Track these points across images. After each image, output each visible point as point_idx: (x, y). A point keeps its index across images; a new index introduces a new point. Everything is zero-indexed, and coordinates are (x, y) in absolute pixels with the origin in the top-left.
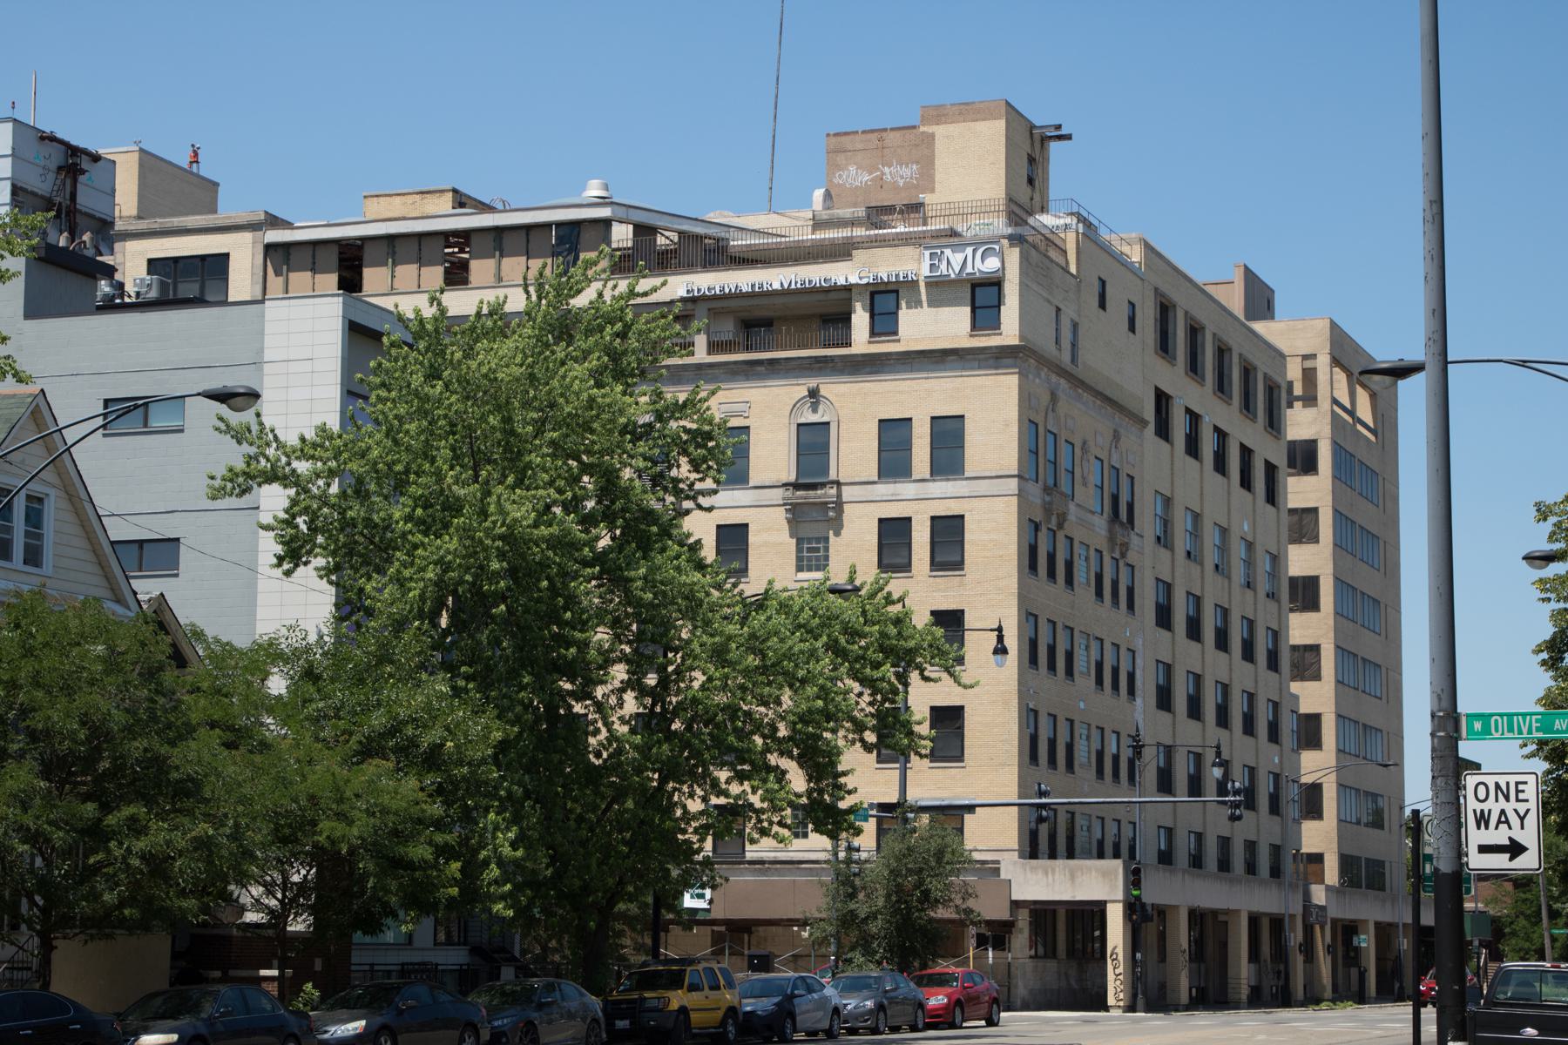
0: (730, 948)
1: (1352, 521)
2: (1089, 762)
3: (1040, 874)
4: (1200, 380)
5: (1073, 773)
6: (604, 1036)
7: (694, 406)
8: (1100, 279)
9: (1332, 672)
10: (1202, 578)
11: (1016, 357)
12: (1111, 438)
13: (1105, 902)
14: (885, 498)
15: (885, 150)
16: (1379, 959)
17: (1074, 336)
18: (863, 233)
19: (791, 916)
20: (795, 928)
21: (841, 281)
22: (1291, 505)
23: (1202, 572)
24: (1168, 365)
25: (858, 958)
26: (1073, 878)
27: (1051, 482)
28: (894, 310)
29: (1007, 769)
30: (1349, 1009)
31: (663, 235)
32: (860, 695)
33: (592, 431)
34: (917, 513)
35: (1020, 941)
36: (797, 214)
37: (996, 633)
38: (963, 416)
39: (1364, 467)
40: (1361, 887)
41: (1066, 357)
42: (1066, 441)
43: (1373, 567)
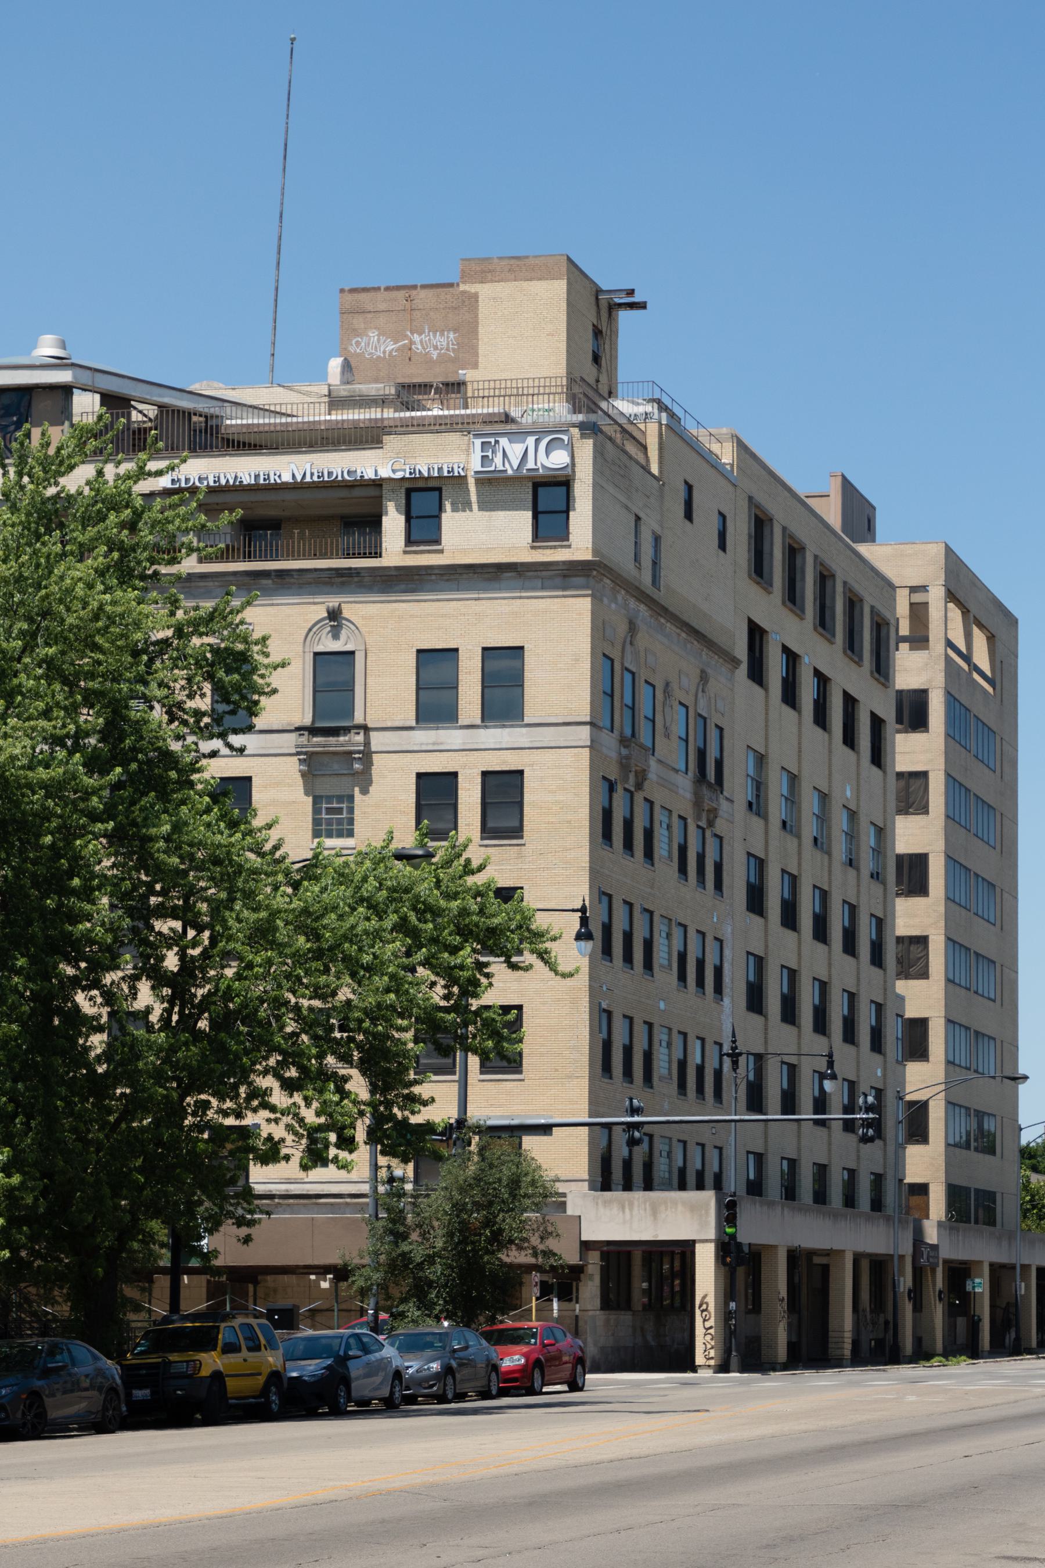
0: (232, 1301)
1: (966, 789)
2: (670, 1073)
3: (615, 1209)
4: (798, 612)
5: (652, 1087)
6: (124, 1409)
7: (225, 618)
8: (686, 482)
9: (942, 968)
10: (800, 853)
11: (588, 576)
12: (697, 680)
13: (694, 1242)
14: (424, 748)
15: (414, 313)
16: (993, 1306)
17: (656, 551)
18: (391, 415)
19: (309, 1262)
20: (313, 1277)
21: (370, 475)
22: (899, 768)
23: (800, 845)
24: (762, 591)
25: (412, 1310)
26: (655, 1213)
27: (628, 732)
28: (436, 513)
29: (575, 1081)
30: (963, 1364)
31: (135, 408)
32: (433, 984)
33: (96, 647)
34: (464, 767)
35: (590, 1290)
36: (309, 389)
37: (579, 914)
38: (522, 648)
39: (980, 725)
40: (970, 1222)
41: (646, 578)
42: (646, 682)
43: (988, 844)
